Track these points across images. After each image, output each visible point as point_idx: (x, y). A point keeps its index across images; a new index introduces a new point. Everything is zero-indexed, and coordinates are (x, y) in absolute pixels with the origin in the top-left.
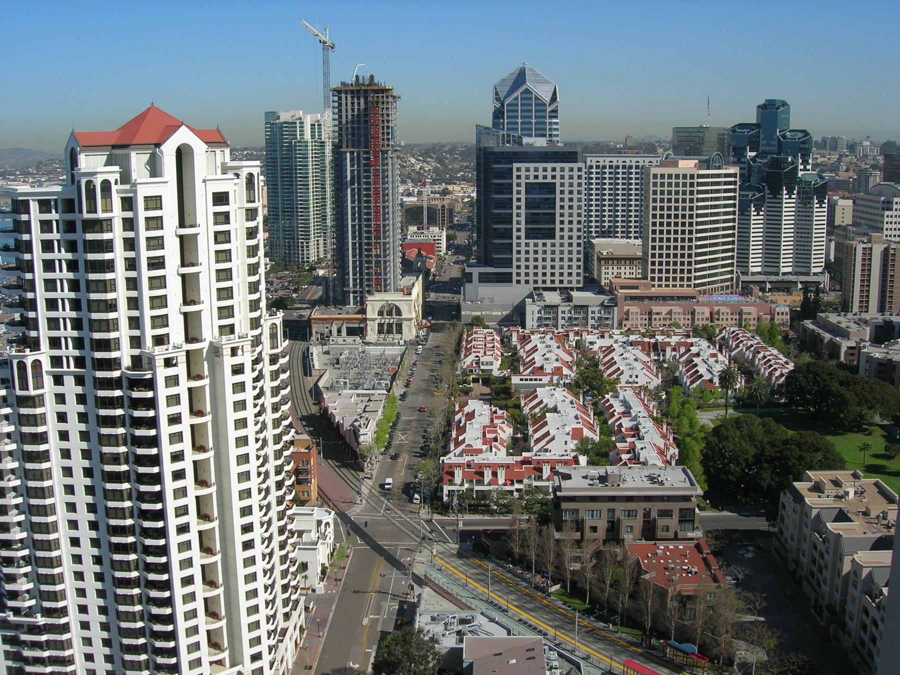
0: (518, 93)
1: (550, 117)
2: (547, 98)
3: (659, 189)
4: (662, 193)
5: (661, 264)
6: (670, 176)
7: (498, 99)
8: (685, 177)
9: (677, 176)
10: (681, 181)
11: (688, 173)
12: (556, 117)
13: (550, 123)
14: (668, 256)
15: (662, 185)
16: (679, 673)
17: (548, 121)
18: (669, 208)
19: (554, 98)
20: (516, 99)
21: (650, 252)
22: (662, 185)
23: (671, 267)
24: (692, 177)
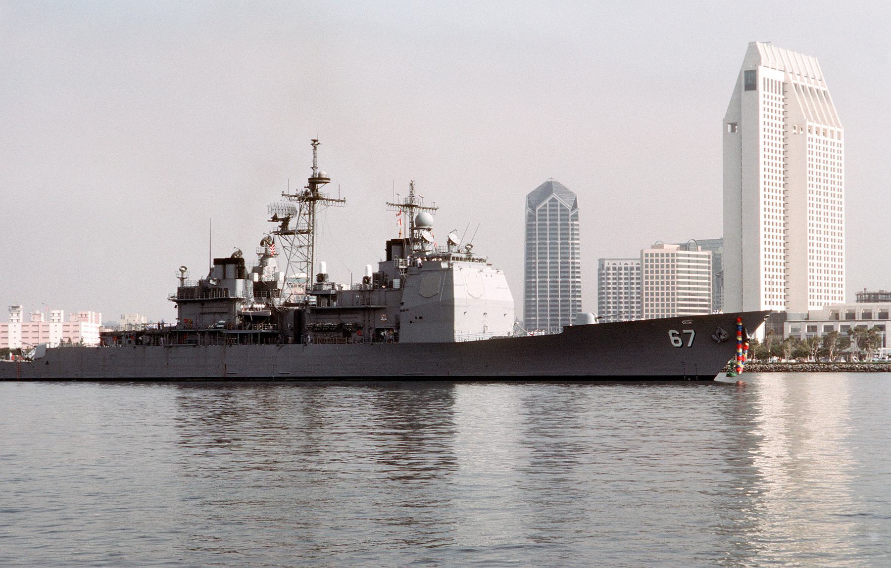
0: (547, 201)
1: (572, 220)
2: (569, 206)
3: (649, 280)
4: (652, 277)
5: (652, 272)
6: (657, 255)
7: (531, 206)
8: (668, 255)
9: (662, 255)
10: (665, 258)
11: (670, 252)
12: (577, 220)
13: (572, 225)
14: (657, 294)
15: (652, 261)
16: (529, 197)
17: (570, 223)
18: (657, 277)
19: (575, 206)
20: (546, 205)
21: (644, 258)
22: (652, 261)
23: (660, 291)
24: (673, 255)
